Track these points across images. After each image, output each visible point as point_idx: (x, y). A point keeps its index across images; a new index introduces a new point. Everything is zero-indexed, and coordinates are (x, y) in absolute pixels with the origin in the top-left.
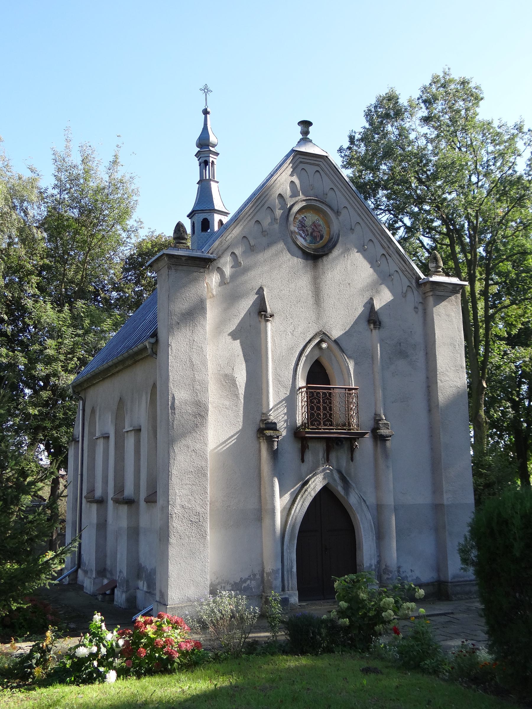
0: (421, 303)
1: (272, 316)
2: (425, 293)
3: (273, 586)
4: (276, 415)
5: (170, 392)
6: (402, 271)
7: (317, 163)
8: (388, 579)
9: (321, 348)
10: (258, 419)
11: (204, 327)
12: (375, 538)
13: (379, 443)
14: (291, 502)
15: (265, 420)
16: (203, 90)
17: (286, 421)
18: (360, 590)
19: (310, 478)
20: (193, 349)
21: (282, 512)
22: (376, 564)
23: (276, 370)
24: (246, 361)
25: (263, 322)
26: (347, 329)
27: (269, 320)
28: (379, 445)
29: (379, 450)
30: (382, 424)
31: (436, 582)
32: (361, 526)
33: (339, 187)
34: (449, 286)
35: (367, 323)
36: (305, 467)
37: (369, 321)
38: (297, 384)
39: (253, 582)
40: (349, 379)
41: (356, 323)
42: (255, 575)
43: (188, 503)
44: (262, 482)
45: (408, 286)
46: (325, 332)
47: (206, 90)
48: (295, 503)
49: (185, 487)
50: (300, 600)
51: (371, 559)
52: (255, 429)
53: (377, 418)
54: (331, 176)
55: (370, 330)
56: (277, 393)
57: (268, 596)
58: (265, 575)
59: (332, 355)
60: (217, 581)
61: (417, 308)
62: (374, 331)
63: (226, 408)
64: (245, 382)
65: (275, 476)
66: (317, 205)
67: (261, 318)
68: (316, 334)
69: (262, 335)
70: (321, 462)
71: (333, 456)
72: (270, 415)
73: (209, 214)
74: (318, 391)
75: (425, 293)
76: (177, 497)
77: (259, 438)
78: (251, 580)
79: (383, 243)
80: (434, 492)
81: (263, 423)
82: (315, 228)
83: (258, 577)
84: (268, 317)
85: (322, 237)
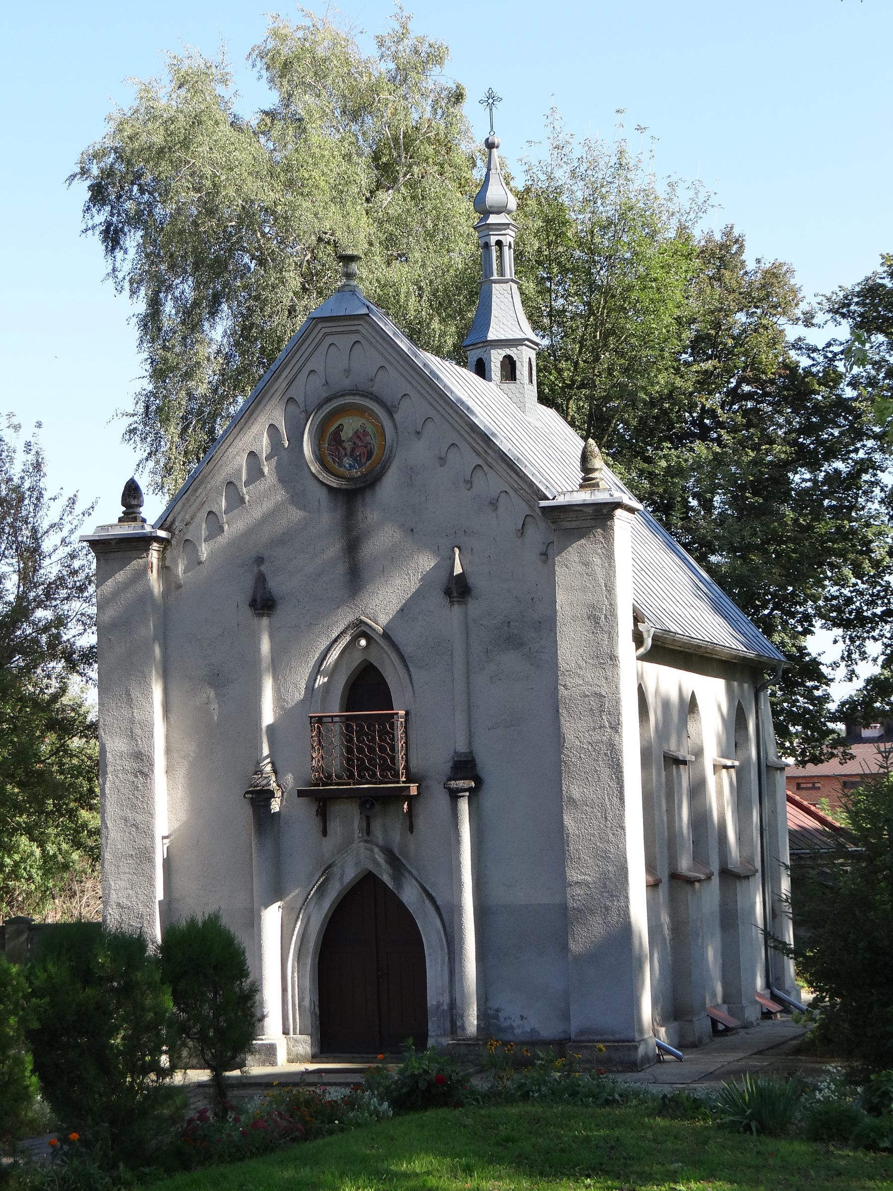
6: (515, 490)
7: (353, 328)
33: (394, 362)
34: (585, 509)
49: (122, 876)
54: (379, 347)
59: (385, 655)
70: (356, 835)
71: (377, 827)
73: (484, 349)
76: (112, 892)
79: (478, 447)
82: (357, 441)
85: (370, 454)
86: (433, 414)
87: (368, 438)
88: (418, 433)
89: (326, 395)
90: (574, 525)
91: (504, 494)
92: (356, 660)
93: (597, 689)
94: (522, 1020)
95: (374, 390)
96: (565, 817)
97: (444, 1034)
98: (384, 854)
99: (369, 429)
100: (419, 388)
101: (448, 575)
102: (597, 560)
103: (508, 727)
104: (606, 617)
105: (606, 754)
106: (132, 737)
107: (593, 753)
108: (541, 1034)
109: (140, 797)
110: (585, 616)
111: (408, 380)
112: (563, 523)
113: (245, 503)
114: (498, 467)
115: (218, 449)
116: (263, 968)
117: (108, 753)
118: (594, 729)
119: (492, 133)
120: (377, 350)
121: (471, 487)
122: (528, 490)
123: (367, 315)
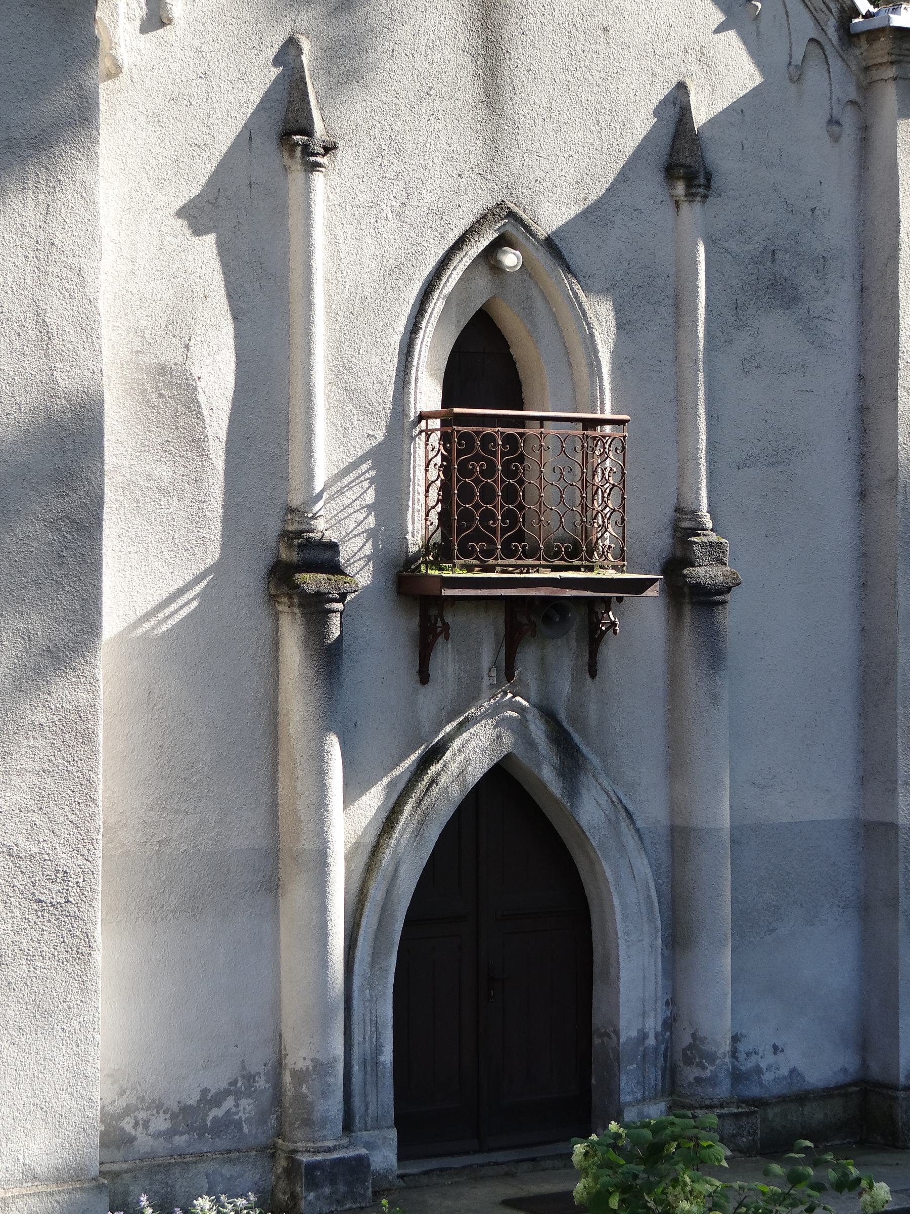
0: (852, 102)
1: (328, 149)
2: (867, 69)
3: (316, 1116)
4: (334, 512)
8: (698, 1080)
9: (497, 269)
10: (273, 527)
11: (89, 200)
12: (659, 941)
13: (687, 610)
14: (379, 824)
15: (298, 534)
17: (372, 534)
18: (679, 1188)
19: (450, 738)
20: (50, 278)
21: (348, 859)
22: (659, 1029)
23: (339, 348)
24: (236, 317)
25: (297, 173)
26: (593, 197)
27: (320, 165)
28: (688, 619)
29: (687, 636)
30: (703, 545)
31: (854, 1083)
32: (616, 902)
35: (660, 177)
38: (412, 400)
39: (244, 1102)
40: (593, 382)
41: (623, 176)
42: (250, 1078)
43: (29, 836)
44: (283, 756)
45: (812, 40)
46: (516, 209)
48: (393, 828)
49: (16, 780)
50: (401, 1158)
51: (644, 1014)
52: (261, 566)
53: (685, 524)
55: (672, 205)
56: (342, 434)
57: (295, 1151)
58: (287, 1078)
59: (535, 292)
60: (122, 1103)
61: (838, 123)
62: (685, 207)
63: (160, 490)
64: (230, 393)
65: (328, 729)
67: (292, 156)
68: (484, 217)
69: (295, 219)
70: (486, 682)
72: (314, 517)
74: (489, 430)
75: (867, 69)
77: (273, 599)
78: (238, 1095)
80: (863, 781)
81: (290, 546)
83: (261, 1083)
94: (775, 1053)
103: (773, 464)
108: (807, 1079)
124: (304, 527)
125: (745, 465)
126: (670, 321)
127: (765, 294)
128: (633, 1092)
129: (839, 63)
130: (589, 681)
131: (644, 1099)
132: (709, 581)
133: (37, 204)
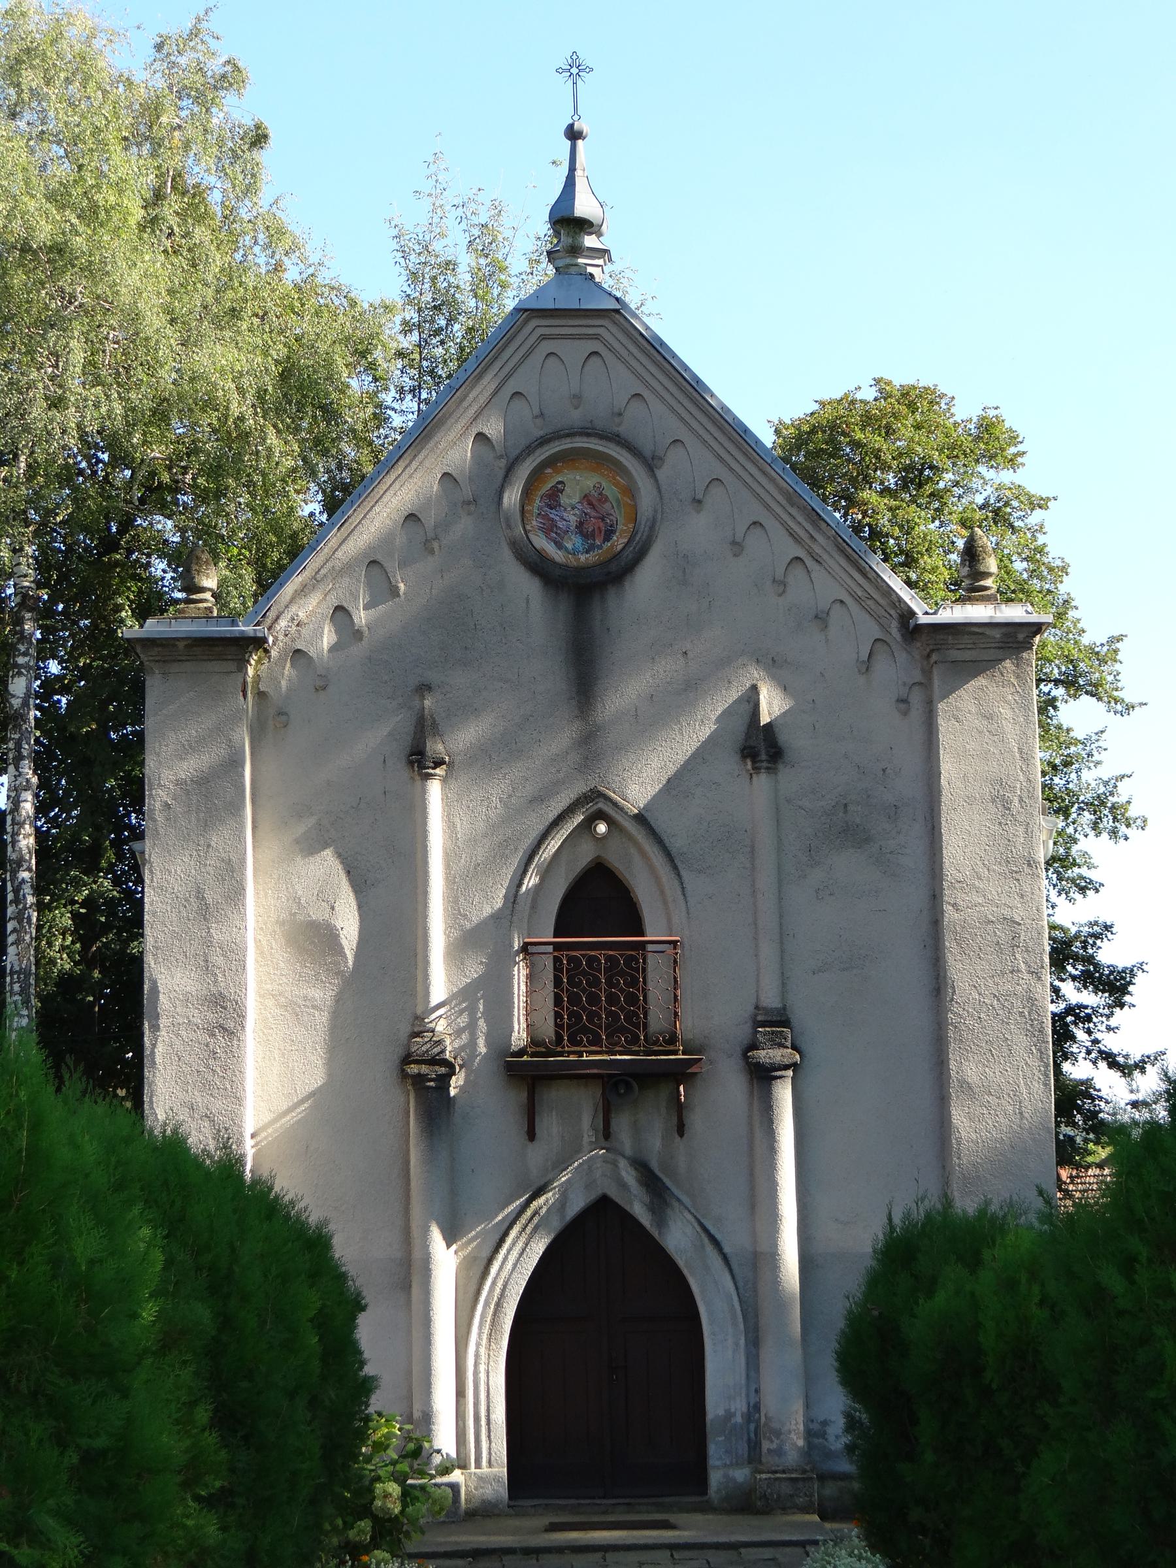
5: (146, 974)
6: (858, 599)
16: (565, 70)
25: (419, 783)
27: (432, 775)
33: (659, 388)
34: (988, 631)
35: (737, 757)
36: (537, 1155)
37: (748, 753)
47: (575, 69)
59: (633, 851)
63: (314, 1007)
66: (591, 446)
70: (586, 1140)
71: (622, 1124)
84: (428, 768)
86: (721, 471)
87: (607, 506)
88: (699, 502)
89: (541, 433)
90: (968, 655)
91: (838, 605)
92: (585, 854)
93: (1006, 912)
95: (622, 430)
96: (953, 1112)
97: (737, 1464)
98: (636, 1169)
99: (611, 491)
100: (702, 432)
101: (743, 728)
102: (1006, 712)
104: (1021, 800)
105: (1021, 1014)
106: (207, 967)
107: (1000, 1012)
109: (218, 1069)
110: (987, 797)
111: (682, 419)
112: (951, 651)
113: (398, 595)
114: (831, 562)
115: (359, 506)
116: (434, 1357)
117: (161, 996)
118: (1003, 973)
119: (576, 118)
120: (629, 367)
121: (784, 591)
122: (881, 601)
123: (617, 311)
124: (421, 1029)
125: (820, 971)
126: (748, 865)
127: (838, 838)
128: (720, 1458)
129: (904, 655)
130: (678, 1139)
131: (732, 1464)
132: (768, 1061)
133: (198, 820)
